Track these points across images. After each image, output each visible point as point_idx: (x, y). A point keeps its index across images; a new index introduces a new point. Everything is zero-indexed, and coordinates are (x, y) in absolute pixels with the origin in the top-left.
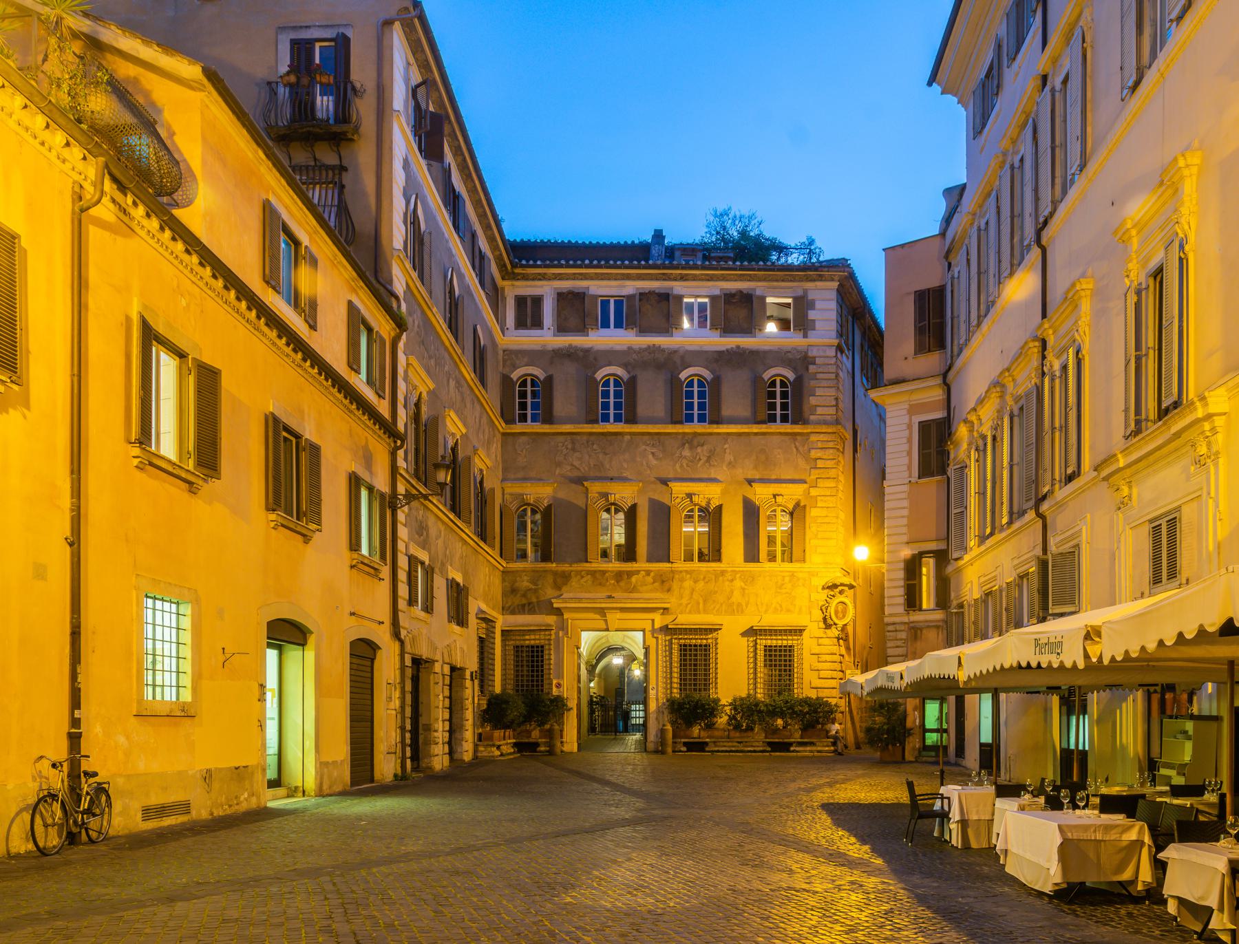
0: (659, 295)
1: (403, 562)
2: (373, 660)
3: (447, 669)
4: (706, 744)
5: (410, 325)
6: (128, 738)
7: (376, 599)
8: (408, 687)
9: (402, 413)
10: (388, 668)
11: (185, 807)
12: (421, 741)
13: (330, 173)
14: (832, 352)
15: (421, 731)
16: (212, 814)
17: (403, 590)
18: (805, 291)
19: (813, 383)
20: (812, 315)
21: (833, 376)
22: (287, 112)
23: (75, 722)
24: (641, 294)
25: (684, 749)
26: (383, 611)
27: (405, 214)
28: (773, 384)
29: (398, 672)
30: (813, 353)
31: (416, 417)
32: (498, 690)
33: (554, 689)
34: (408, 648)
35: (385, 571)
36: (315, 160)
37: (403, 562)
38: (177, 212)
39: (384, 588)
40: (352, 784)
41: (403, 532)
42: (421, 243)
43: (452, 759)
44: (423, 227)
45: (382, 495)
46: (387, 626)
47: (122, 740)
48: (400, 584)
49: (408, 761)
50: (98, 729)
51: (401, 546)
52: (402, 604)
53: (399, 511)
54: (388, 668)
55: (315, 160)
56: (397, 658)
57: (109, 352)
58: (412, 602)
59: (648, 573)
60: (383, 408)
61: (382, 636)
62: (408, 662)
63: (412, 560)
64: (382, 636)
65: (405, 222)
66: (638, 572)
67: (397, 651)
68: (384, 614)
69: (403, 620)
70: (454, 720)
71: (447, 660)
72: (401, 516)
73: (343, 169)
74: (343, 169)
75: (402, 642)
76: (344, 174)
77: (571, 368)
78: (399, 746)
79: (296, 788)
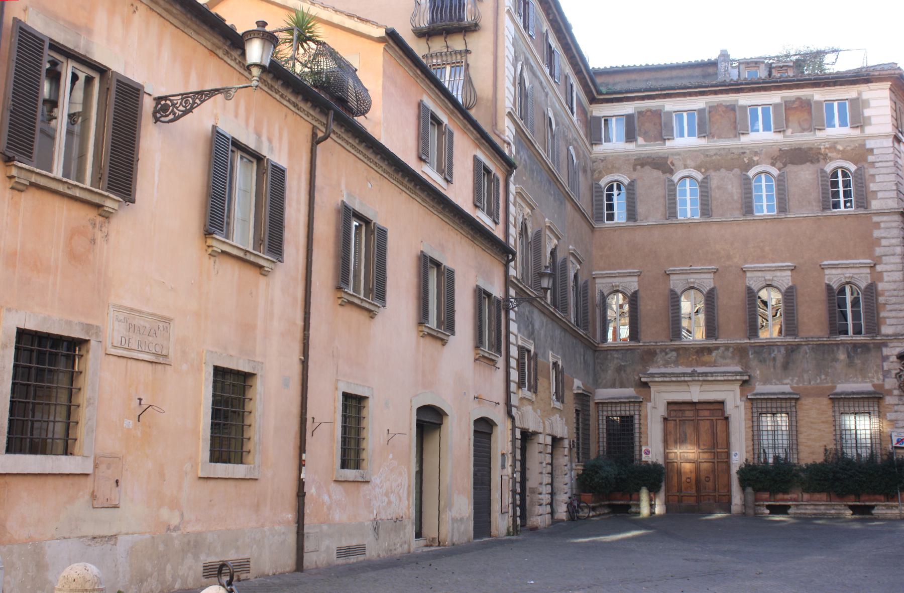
0: (727, 107)
1: (514, 352)
2: (490, 434)
3: (549, 440)
4: (789, 507)
5: (517, 163)
6: (330, 497)
7: (493, 384)
8: (518, 457)
9: (512, 231)
10: (457, 436)
11: (361, 549)
12: (528, 502)
13: (459, 57)
14: (889, 142)
15: (528, 493)
16: (379, 556)
17: (514, 375)
18: (860, 94)
19: (872, 171)
20: (867, 112)
21: (892, 164)
22: (427, 16)
23: (301, 484)
24: (710, 107)
25: (768, 511)
26: (498, 394)
27: (515, 78)
28: (835, 175)
29: (510, 444)
30: (870, 144)
31: (523, 231)
32: (593, 456)
33: (644, 455)
34: (518, 424)
35: (501, 362)
36: (447, 47)
37: (514, 352)
38: (360, 120)
39: (500, 374)
40: (475, 537)
41: (513, 327)
42: (526, 96)
43: (552, 517)
44: (527, 84)
45: (499, 301)
46: (502, 408)
47: (326, 498)
48: (512, 370)
49: (518, 519)
50: (313, 490)
51: (512, 339)
52: (513, 387)
53: (511, 312)
54: (502, 441)
55: (447, 47)
56: (510, 432)
57: (325, 229)
58: (521, 384)
59: (727, 347)
60: (498, 233)
61: (497, 415)
62: (518, 435)
63: (522, 350)
64: (497, 415)
65: (514, 85)
66: (717, 348)
67: (510, 426)
68: (500, 396)
69: (514, 400)
70: (555, 484)
71: (548, 431)
72: (512, 315)
73: (467, 52)
74: (467, 52)
75: (513, 418)
76: (468, 55)
77: (651, 175)
78: (511, 506)
79: (433, 539)
